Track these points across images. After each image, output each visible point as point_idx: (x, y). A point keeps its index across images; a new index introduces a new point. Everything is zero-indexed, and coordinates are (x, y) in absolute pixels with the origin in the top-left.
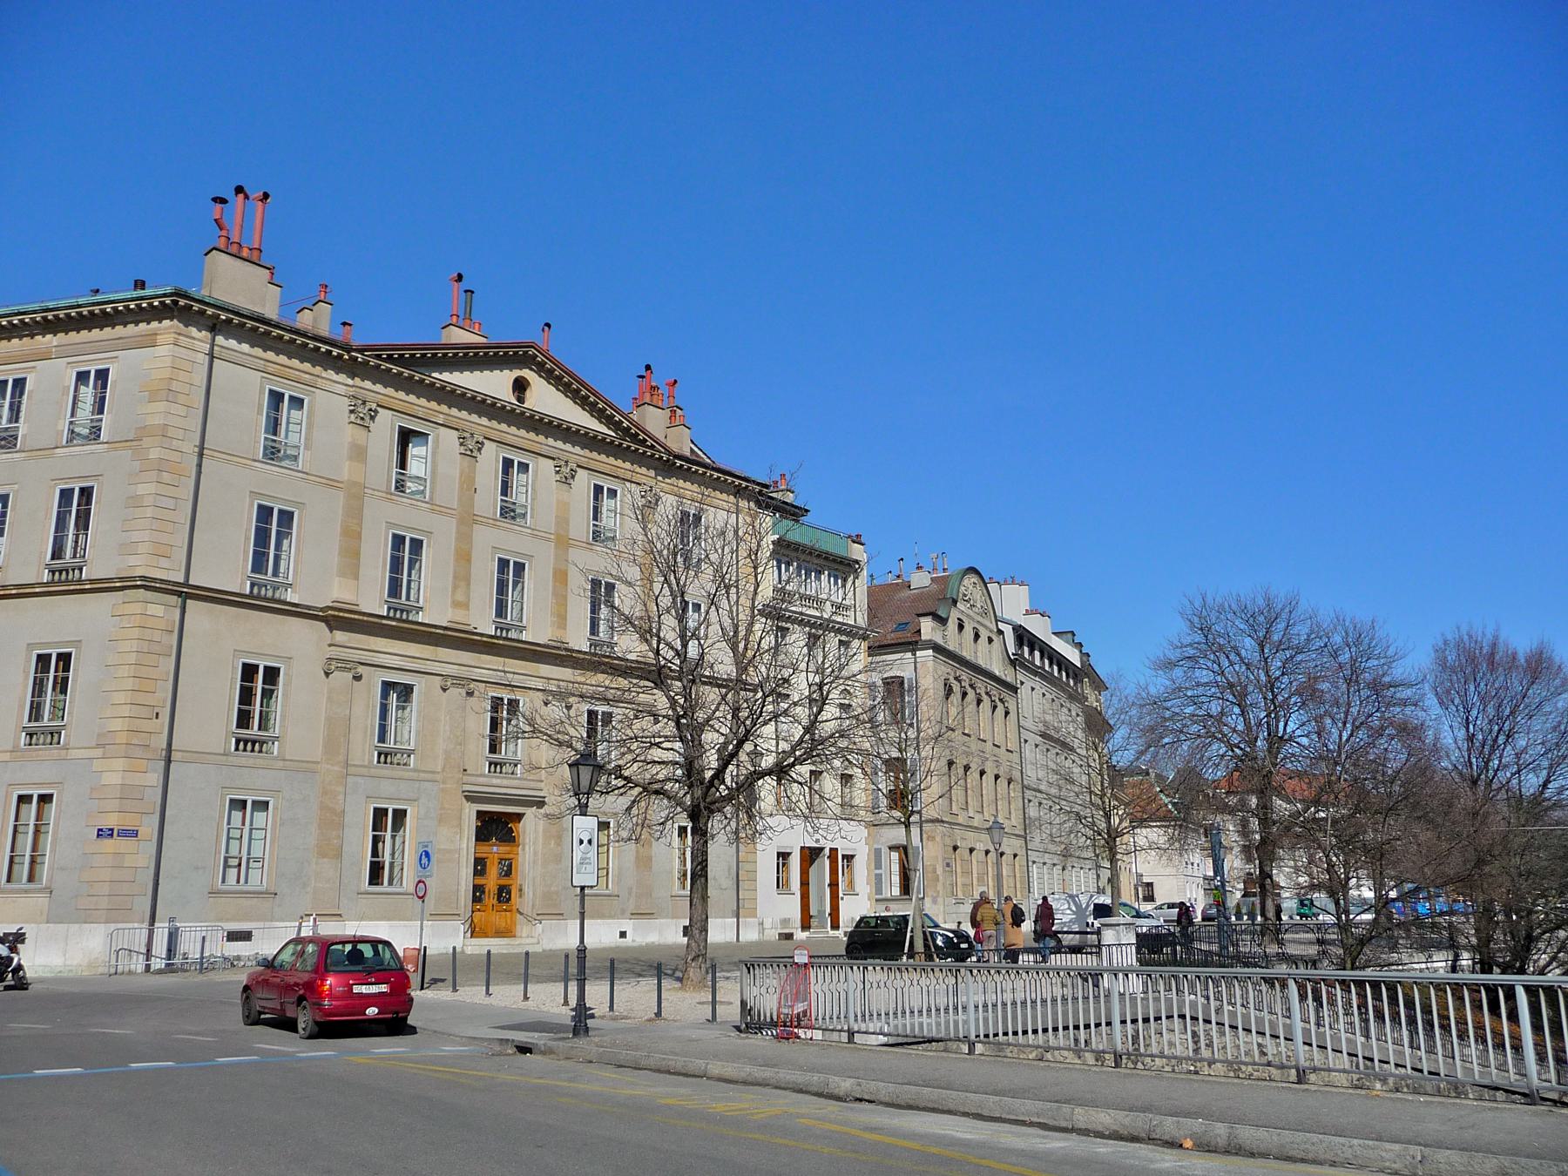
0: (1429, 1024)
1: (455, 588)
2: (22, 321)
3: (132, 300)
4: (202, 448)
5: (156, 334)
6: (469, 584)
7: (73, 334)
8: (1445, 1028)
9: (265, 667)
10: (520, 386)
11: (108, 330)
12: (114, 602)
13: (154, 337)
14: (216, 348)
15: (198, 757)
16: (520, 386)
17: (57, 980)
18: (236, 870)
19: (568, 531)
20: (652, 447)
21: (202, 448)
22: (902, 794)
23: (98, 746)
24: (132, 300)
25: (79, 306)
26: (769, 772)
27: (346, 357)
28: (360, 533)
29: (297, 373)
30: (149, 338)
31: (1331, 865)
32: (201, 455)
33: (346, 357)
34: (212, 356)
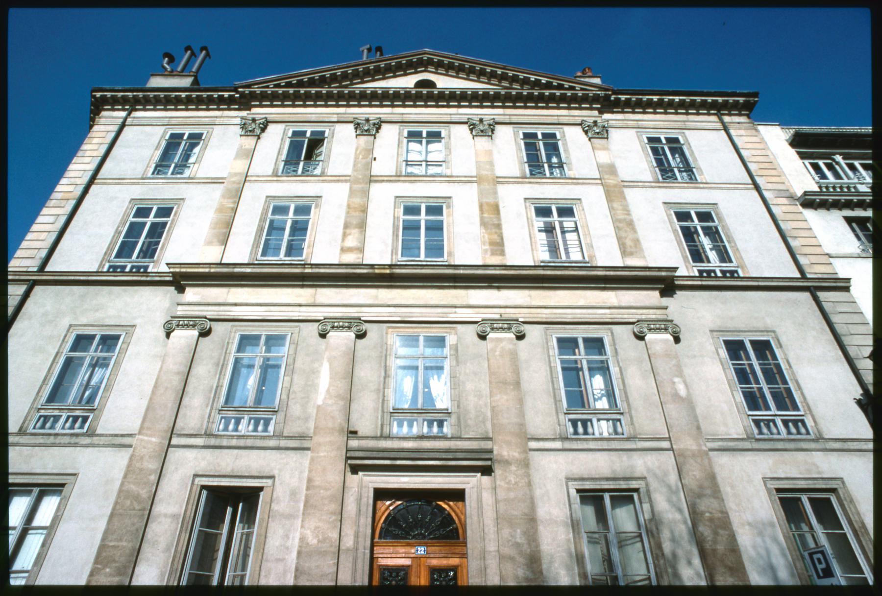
27: (237, 96)
33: (237, 96)
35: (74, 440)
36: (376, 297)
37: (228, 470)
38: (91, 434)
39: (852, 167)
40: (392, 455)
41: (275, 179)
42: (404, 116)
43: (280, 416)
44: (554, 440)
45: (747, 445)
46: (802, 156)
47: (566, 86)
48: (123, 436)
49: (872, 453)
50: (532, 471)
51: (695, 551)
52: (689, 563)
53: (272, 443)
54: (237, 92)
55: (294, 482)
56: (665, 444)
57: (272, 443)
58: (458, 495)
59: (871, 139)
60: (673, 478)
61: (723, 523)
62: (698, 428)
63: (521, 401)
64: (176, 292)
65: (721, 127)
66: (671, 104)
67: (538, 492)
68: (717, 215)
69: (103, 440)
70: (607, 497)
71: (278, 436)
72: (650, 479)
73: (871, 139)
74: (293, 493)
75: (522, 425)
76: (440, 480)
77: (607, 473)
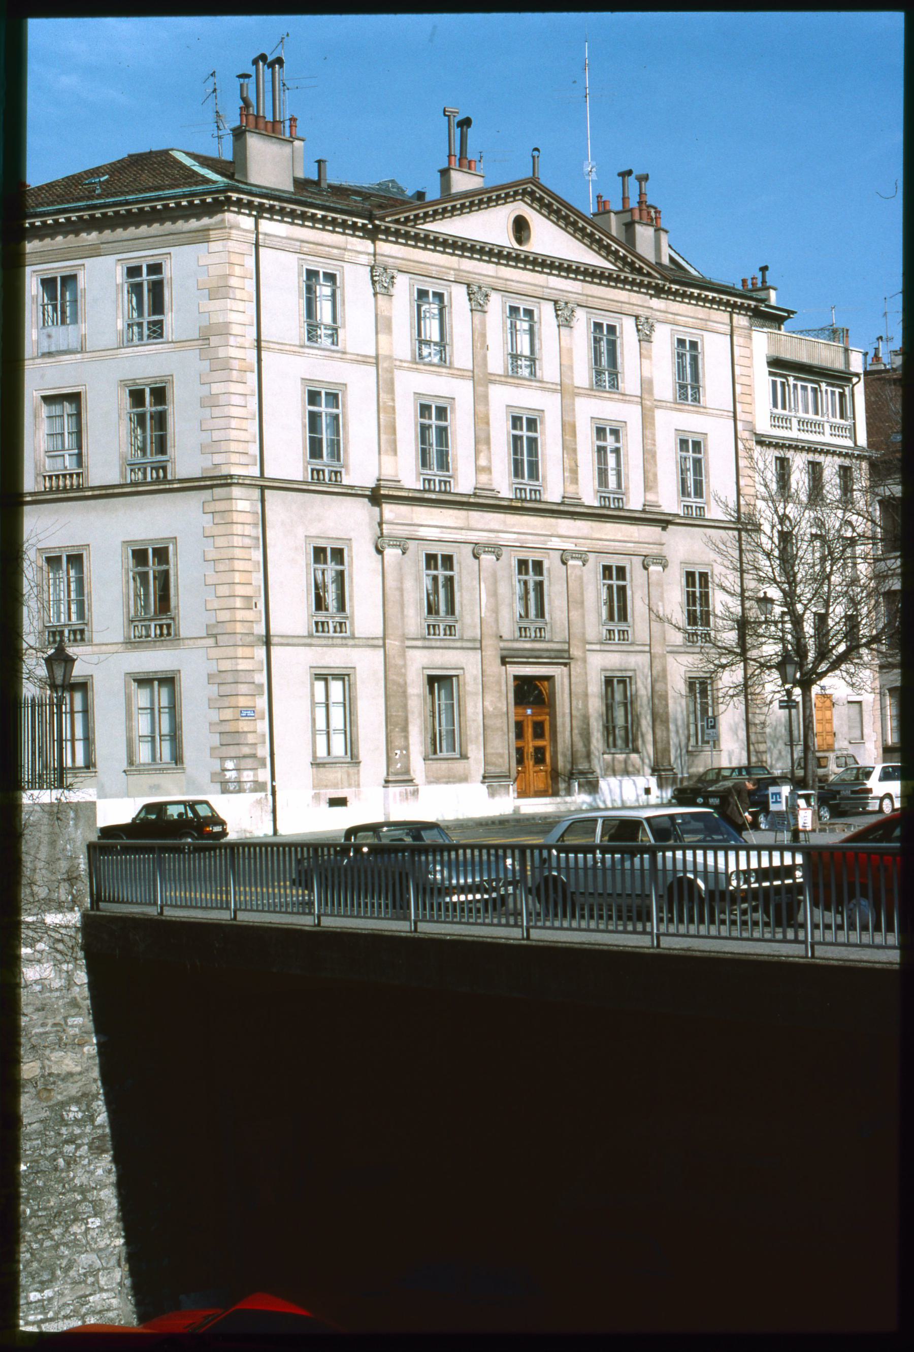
0: (140, 879)
1: (477, 452)
2: (68, 219)
3: (184, 196)
4: (259, 340)
5: (209, 230)
6: (489, 448)
7: (119, 230)
8: (126, 879)
9: (332, 549)
10: (521, 227)
11: (156, 226)
12: (203, 499)
13: (206, 233)
14: (261, 236)
15: (290, 641)
16: (521, 227)
17: (328, 839)
18: (162, 705)
19: (572, 378)
20: (649, 275)
21: (259, 340)
22: (878, 409)
23: (209, 636)
24: (184, 196)
25: (127, 203)
26: (783, 636)
27: (370, 226)
28: (393, 408)
29: (327, 249)
30: (201, 234)
31: (84, 1213)
32: (259, 348)
33: (370, 226)
34: (257, 245)
35: (344, 642)
36: (504, 522)
37: (439, 664)
38: (353, 637)
39: (795, 386)
40: (537, 654)
41: (415, 366)
42: (509, 283)
43: (459, 622)
44: (596, 644)
45: (682, 649)
46: (771, 374)
47: (645, 271)
48: (373, 638)
49: (25, 491)
50: (588, 667)
51: (649, 712)
52: (646, 718)
53: (458, 644)
54: (371, 222)
55: (475, 672)
56: (647, 648)
57: (458, 644)
58: (549, 679)
59: (898, 845)
60: (647, 670)
61: (664, 697)
62: (664, 639)
63: (583, 616)
64: (370, 504)
65: (728, 332)
66: (706, 300)
67: (589, 678)
68: (705, 446)
69: (361, 642)
70: (615, 680)
71: (462, 639)
72: (638, 673)
73: (898, 845)
74: (475, 679)
75: (584, 634)
76: (534, 669)
77: (618, 666)
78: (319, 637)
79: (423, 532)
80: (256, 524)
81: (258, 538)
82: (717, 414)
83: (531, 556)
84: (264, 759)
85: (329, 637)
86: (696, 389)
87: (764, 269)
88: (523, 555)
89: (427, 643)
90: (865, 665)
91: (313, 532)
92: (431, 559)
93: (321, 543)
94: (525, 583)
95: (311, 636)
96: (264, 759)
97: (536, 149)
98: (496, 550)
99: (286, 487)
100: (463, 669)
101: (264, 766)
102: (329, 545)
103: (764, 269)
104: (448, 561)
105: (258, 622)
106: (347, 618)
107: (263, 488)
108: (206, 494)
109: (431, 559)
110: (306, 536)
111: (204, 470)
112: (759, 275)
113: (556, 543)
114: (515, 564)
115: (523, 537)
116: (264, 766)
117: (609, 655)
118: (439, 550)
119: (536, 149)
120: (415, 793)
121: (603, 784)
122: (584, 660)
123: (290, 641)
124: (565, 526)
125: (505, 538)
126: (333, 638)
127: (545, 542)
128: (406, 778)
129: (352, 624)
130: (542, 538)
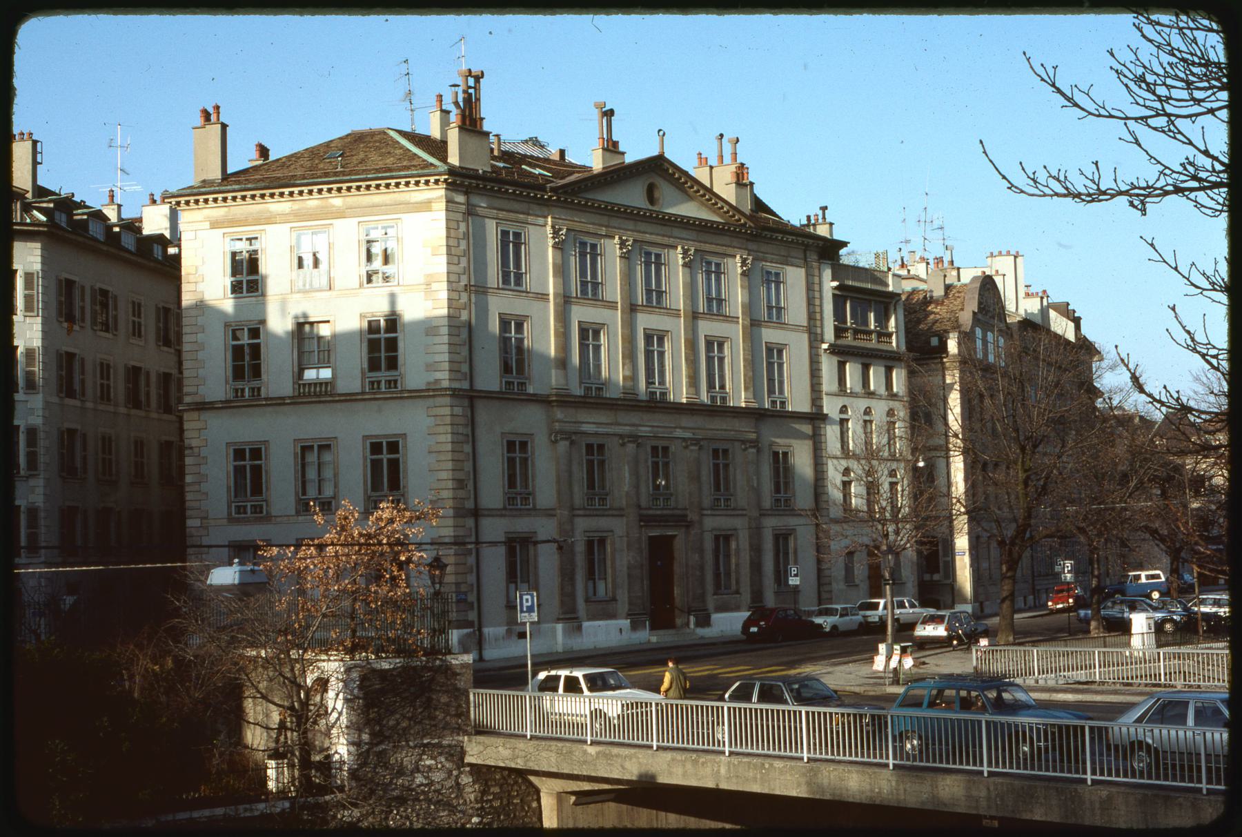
15: (492, 513)
38: (534, 509)
78: (511, 509)
79: (585, 428)
80: (467, 425)
81: (467, 435)
82: (796, 328)
83: (661, 444)
84: (472, 604)
85: (516, 510)
86: (596, 285)
87: (824, 209)
88: (655, 443)
89: (588, 512)
90: (315, 513)
91: (507, 429)
92: (589, 447)
93: (512, 438)
94: (592, 461)
95: (505, 509)
96: (472, 604)
97: (660, 130)
98: (634, 438)
99: (489, 396)
100: (612, 531)
101: (472, 608)
102: (518, 439)
103: (824, 209)
104: (601, 447)
105: (468, 498)
106: (671, 495)
107: (471, 399)
108: (430, 402)
109: (589, 447)
110: (502, 433)
111: (429, 383)
112: (820, 213)
113: (679, 433)
114: (649, 450)
115: (655, 429)
116: (472, 608)
117: (718, 518)
118: (595, 441)
119: (660, 130)
120: (579, 628)
121: (586, 624)
122: (701, 523)
123: (492, 513)
124: (686, 421)
125: (644, 430)
126: (520, 510)
127: (671, 433)
128: (572, 616)
129: (534, 499)
130: (669, 430)
